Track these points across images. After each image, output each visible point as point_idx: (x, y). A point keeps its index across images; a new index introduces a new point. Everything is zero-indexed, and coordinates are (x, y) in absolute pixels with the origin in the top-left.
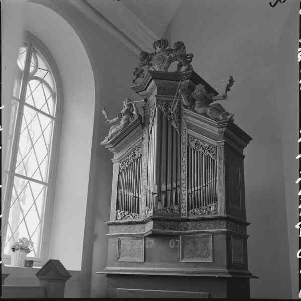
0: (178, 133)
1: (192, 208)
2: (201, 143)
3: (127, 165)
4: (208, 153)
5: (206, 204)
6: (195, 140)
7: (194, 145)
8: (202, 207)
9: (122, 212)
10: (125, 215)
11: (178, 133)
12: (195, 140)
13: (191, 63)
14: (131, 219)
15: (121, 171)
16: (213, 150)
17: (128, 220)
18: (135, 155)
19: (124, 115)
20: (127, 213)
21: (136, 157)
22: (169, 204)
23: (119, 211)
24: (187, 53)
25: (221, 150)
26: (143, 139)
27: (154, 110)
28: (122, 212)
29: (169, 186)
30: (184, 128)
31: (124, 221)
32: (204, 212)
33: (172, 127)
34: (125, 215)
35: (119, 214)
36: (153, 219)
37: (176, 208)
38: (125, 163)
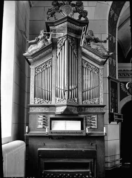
0: (77, 57)
1: (84, 100)
2: (90, 65)
3: (41, 71)
4: (94, 71)
5: (89, 99)
6: (87, 63)
7: (86, 65)
8: (87, 101)
9: (38, 99)
10: (41, 101)
11: (77, 57)
12: (87, 63)
13: (87, 16)
14: (45, 104)
15: (36, 74)
16: (97, 70)
17: (43, 104)
18: (47, 65)
19: (41, 40)
20: (42, 100)
21: (47, 67)
22: (88, 99)
23: (36, 98)
24: (84, 10)
25: (101, 71)
26: (53, 56)
27: (117, 29)
28: (38, 99)
29: (73, 86)
30: (80, 55)
31: (40, 104)
32: (92, 102)
33: (74, 53)
34: (41, 101)
35: (36, 100)
36: (67, 105)
37: (76, 99)
38: (39, 69)
